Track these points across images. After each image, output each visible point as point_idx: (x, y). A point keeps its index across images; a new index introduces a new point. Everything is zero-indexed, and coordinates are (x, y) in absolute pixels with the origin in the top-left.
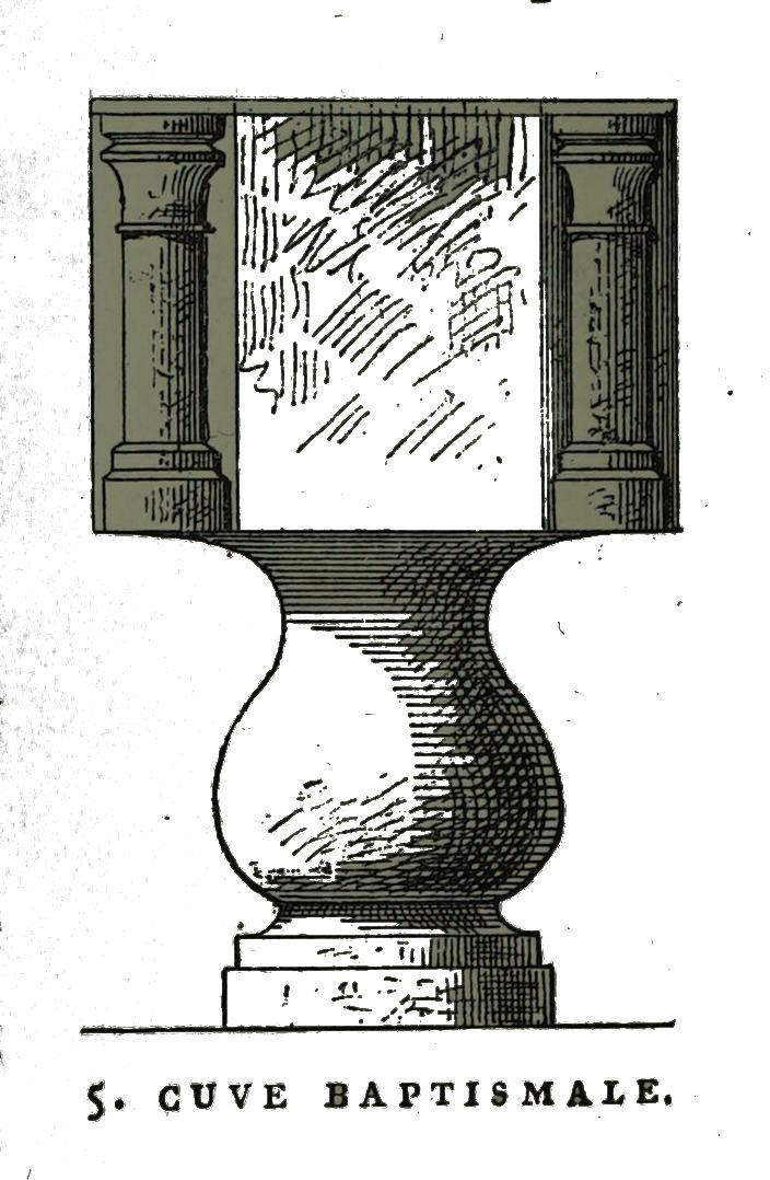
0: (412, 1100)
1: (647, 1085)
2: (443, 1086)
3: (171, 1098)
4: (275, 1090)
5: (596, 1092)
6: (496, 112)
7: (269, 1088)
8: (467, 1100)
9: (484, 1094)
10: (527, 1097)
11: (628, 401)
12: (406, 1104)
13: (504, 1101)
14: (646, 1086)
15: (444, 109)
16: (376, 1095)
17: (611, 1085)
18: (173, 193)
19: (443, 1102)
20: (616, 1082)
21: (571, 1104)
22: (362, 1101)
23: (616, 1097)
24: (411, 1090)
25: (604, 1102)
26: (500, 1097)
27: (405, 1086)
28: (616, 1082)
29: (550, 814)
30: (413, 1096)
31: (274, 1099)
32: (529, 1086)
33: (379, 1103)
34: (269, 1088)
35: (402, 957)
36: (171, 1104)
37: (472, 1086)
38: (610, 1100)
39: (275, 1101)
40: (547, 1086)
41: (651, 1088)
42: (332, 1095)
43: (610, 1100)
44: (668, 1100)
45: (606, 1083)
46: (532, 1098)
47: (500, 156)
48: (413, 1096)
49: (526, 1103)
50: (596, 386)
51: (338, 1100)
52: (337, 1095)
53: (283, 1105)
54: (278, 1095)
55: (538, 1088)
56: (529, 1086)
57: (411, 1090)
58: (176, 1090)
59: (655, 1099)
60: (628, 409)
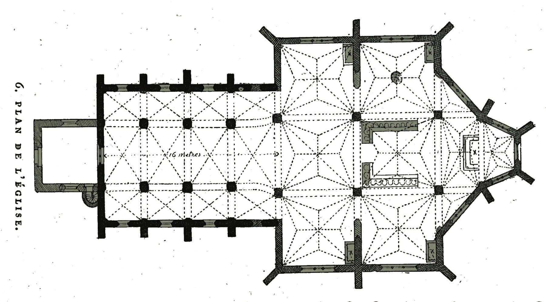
0: (17, 105)
3: (19, 193)
4: (20, 156)
6: (348, 31)
7: (20, 155)
8: (17, 199)
9: (19, 212)
10: (18, 129)
13: (16, 215)
15: (473, 139)
16: (18, 122)
17: (20, 112)
20: (21, 172)
21: (16, 119)
22: (17, 118)
24: (20, 104)
25: (16, 110)
26: (19, 215)
27: (21, 103)
28: (21, 172)
30: (18, 105)
31: (18, 223)
33: (16, 123)
34: (20, 155)
36: (17, 193)
38: (16, 200)
39: (17, 223)
41: (20, 224)
42: (18, 145)
43: (16, 200)
44: (17, 229)
45: (21, 110)
48: (18, 105)
50: (287, 198)
51: (17, 147)
53: (16, 158)
54: (19, 157)
57: (20, 104)
58: (20, 195)
59: (16, 225)
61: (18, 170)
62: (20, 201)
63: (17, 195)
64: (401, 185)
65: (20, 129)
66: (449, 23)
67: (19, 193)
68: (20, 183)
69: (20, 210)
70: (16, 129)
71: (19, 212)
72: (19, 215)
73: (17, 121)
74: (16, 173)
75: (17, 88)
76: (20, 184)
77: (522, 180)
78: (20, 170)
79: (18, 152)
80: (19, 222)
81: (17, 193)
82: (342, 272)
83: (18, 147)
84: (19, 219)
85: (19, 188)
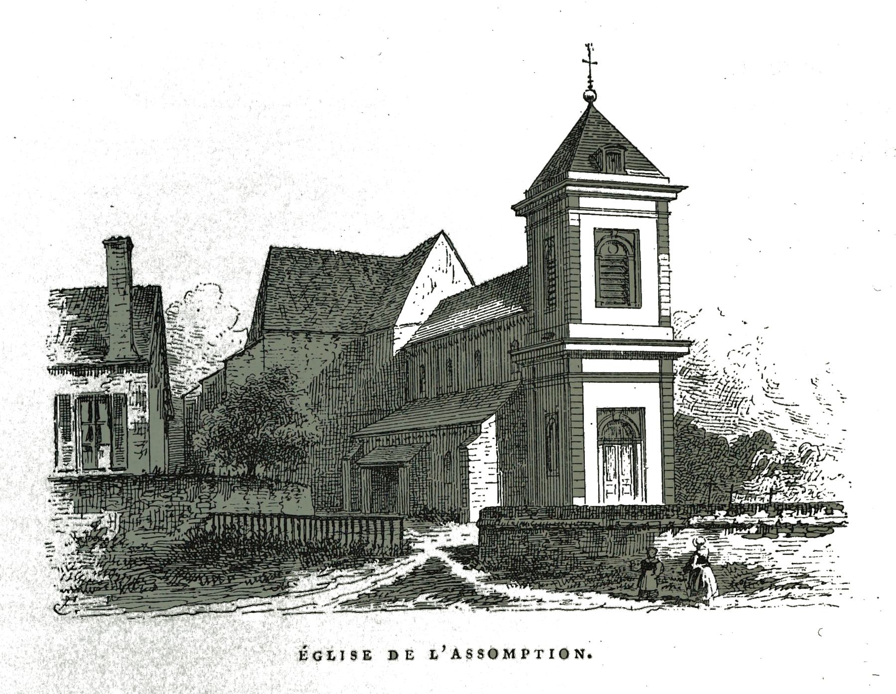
0: (526, 656)
1: (367, 653)
2: (539, 651)
3: (317, 655)
4: (409, 653)
5: (463, 653)
9: (347, 655)
11: (556, 226)
12: (524, 657)
14: (580, 653)
16: (458, 654)
18: (318, 585)
19: (539, 657)
21: (453, 658)
23: (435, 655)
24: (526, 652)
26: (354, 654)
27: (523, 650)
29: (670, 431)
32: (506, 651)
33: (459, 657)
34: (407, 652)
35: (599, 502)
36: (317, 658)
37: (552, 650)
39: (409, 657)
40: (513, 651)
46: (507, 656)
47: (359, 583)
49: (505, 658)
52: (393, 655)
55: (509, 651)
56: (506, 651)
57: (526, 652)
60: (556, 230)
61: (432, 654)
62: (330, 652)
63: (320, 658)
64: (618, 248)
65: (577, 651)
66: (644, 408)
67: (317, 655)
68: (301, 652)
69: (554, 652)
70: (576, 657)
71: (347, 655)
72: (354, 654)
73: (456, 657)
74: (436, 658)
75: (498, 657)
76: (303, 653)
77: (518, 209)
78: (432, 651)
79: (402, 655)
80: (301, 655)
81: (317, 658)
82: (636, 148)
83: (394, 655)
84: (360, 655)
85: (310, 656)
